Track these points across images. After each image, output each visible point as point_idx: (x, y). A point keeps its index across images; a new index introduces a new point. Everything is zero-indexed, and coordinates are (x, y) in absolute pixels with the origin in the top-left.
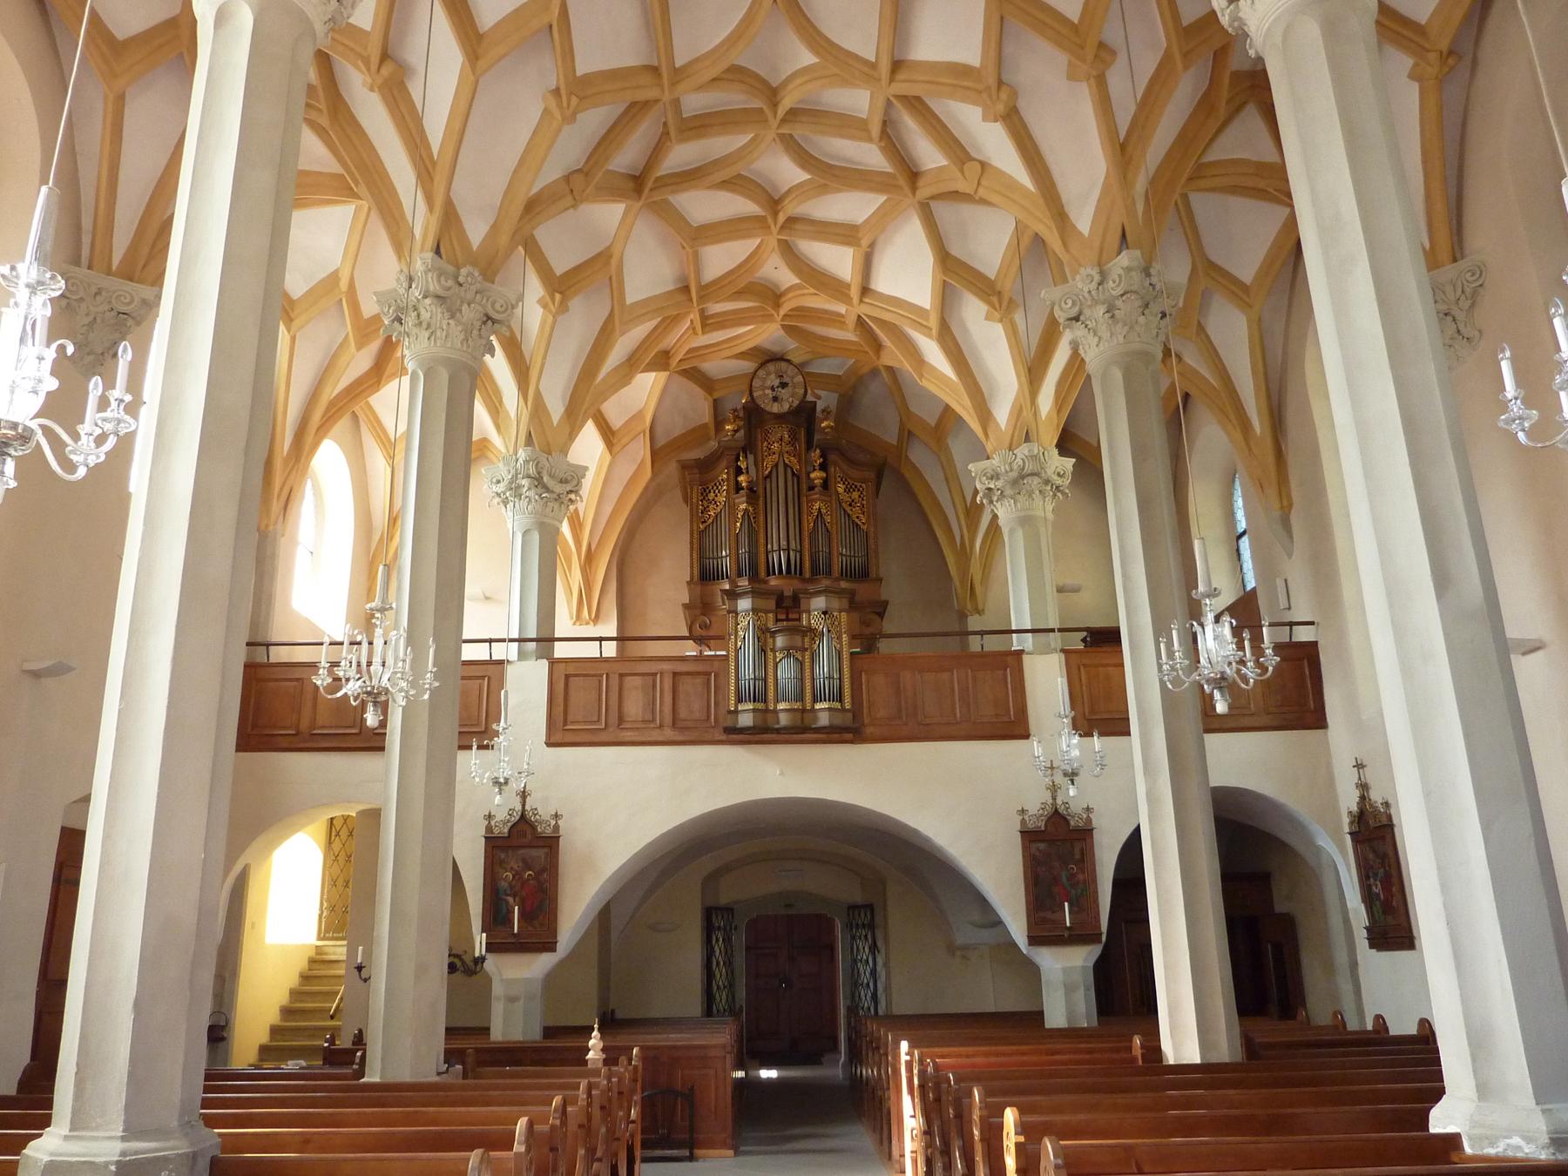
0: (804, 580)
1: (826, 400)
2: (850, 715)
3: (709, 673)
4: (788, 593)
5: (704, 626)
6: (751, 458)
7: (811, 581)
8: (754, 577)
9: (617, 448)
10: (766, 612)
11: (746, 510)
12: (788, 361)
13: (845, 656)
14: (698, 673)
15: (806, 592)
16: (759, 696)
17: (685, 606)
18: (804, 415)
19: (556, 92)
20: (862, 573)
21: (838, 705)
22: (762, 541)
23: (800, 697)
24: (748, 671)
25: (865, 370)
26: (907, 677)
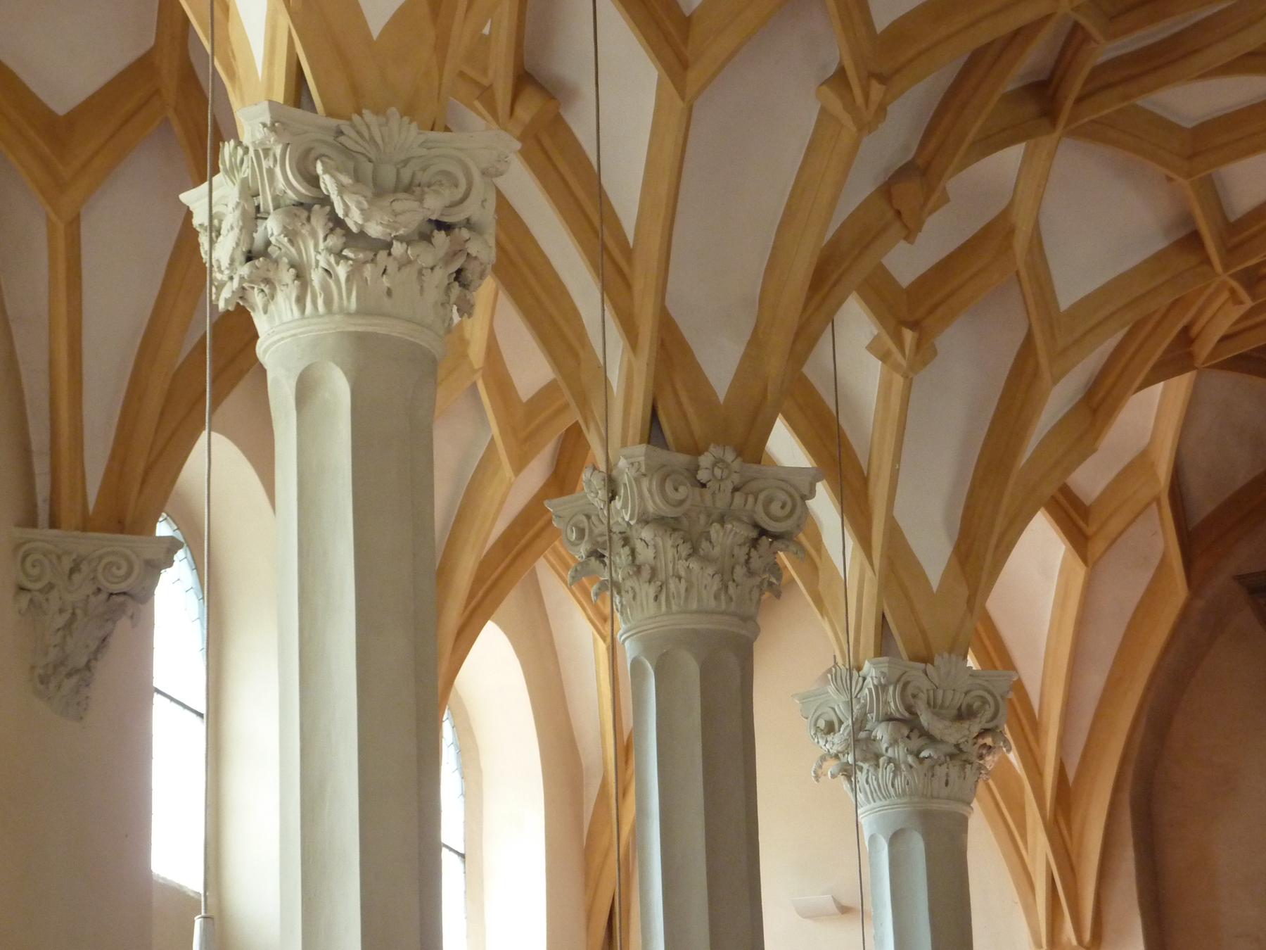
9: (1097, 546)
19: (839, 79)
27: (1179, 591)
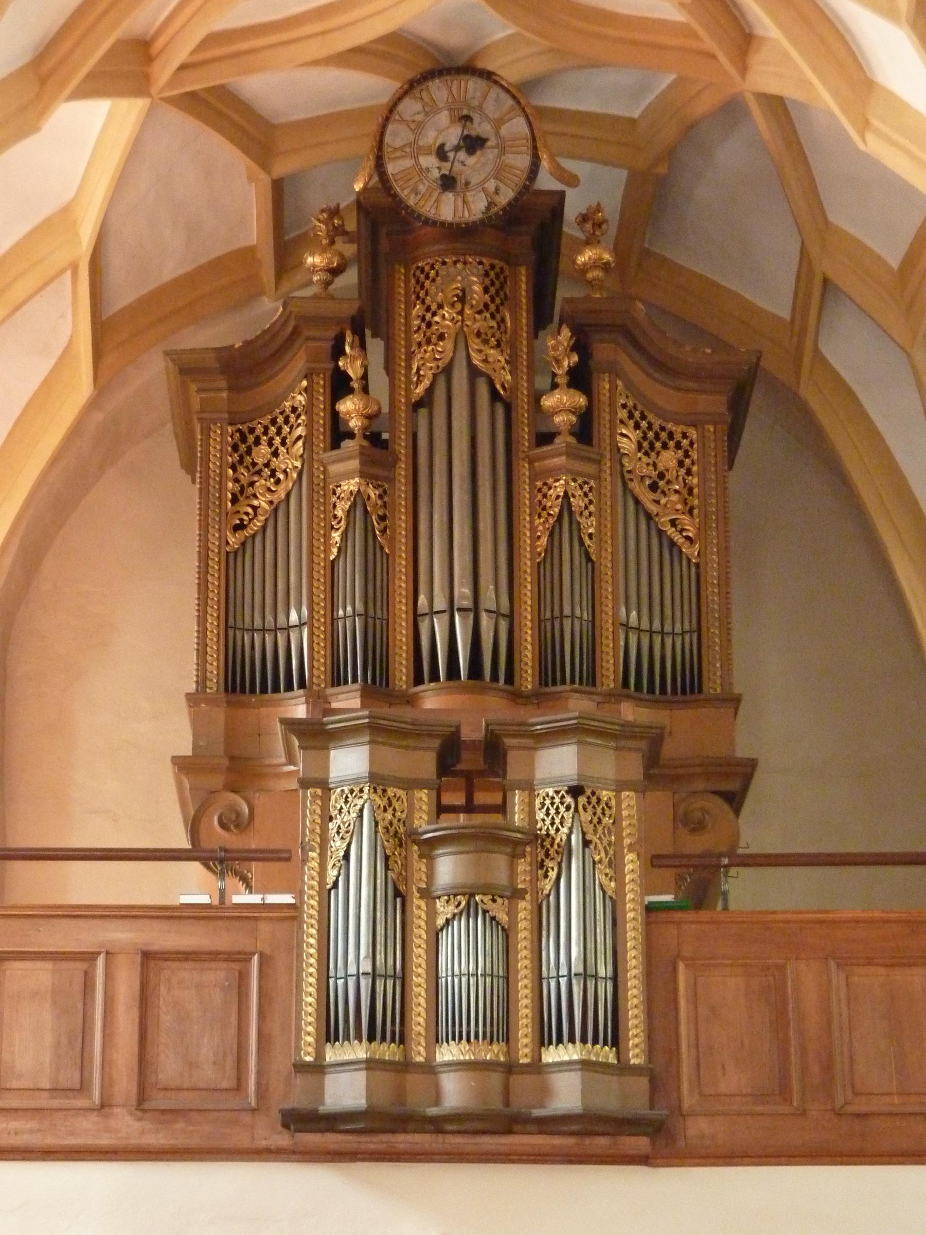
0: (518, 698)
1: (592, 188)
2: (643, 1083)
3: (243, 954)
4: (472, 732)
5: (234, 822)
6: (376, 347)
7: (538, 699)
8: (377, 685)
10: (410, 785)
11: (358, 498)
12: (488, 76)
13: (632, 915)
14: (213, 956)
15: (524, 732)
16: (385, 1024)
17: (182, 765)
18: (528, 232)
20: (682, 681)
21: (607, 1055)
22: (402, 584)
23: (501, 1029)
24: (355, 955)
25: (704, 104)
26: (806, 979)
27: (82, 385)
